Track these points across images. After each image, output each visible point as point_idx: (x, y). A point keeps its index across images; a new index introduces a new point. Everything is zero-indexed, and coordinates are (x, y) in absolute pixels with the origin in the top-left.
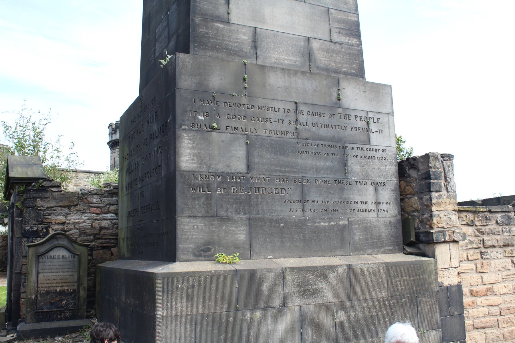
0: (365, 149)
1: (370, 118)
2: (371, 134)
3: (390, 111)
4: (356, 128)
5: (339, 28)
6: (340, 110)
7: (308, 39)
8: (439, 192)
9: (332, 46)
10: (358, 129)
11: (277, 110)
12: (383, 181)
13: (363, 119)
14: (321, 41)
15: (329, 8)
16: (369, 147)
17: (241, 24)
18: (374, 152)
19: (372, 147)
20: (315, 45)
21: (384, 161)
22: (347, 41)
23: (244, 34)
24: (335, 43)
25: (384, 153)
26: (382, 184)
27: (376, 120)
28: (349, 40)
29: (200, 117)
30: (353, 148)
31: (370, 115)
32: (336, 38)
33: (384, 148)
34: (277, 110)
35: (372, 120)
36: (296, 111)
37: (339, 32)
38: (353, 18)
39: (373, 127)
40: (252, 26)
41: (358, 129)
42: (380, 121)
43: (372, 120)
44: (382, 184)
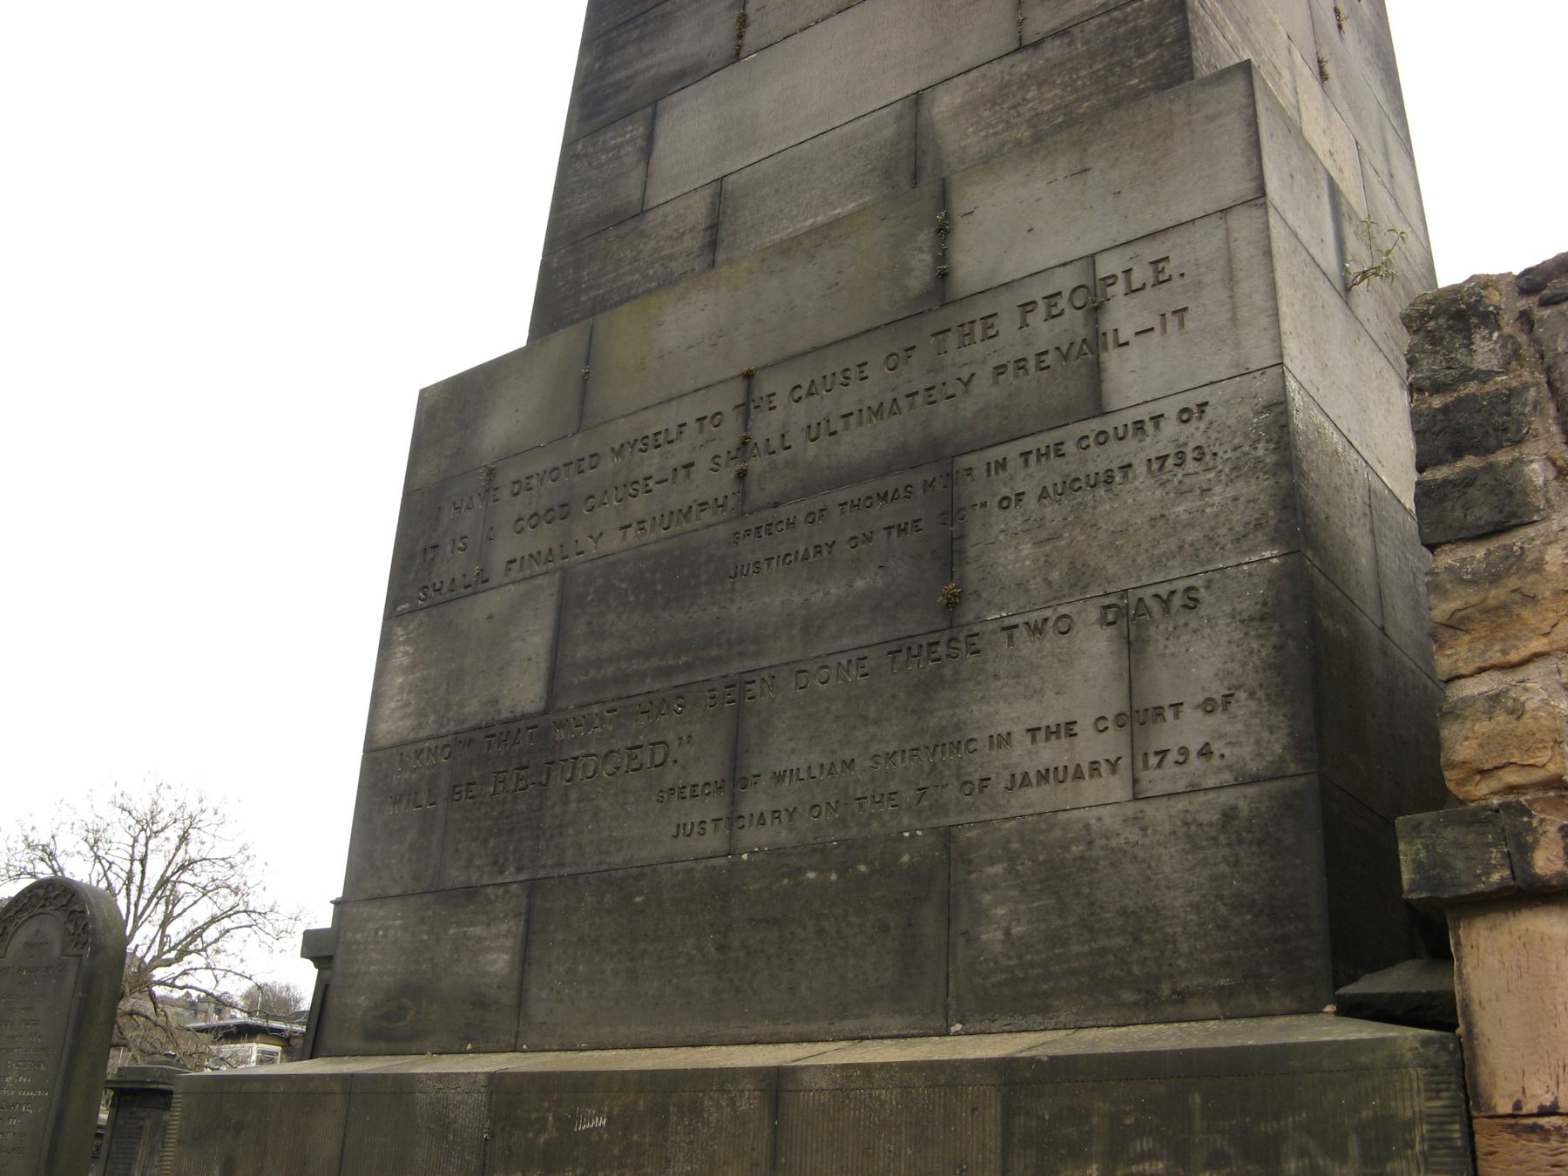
30: (1002, 465)
33: (1191, 400)
35: (1119, 288)
36: (746, 409)
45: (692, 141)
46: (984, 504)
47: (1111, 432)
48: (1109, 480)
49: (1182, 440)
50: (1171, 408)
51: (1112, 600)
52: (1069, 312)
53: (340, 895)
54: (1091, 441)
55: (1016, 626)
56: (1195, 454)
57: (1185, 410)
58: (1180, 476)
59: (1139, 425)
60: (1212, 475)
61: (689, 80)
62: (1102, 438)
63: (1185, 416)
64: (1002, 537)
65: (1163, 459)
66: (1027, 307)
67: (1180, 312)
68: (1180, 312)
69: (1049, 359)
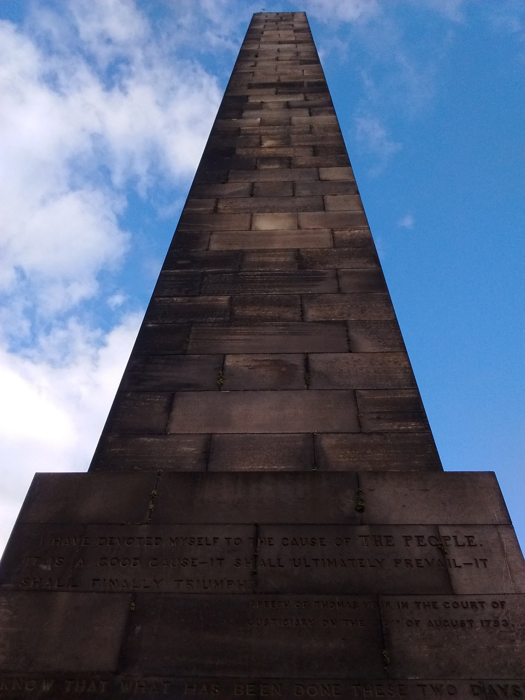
0: (440, 604)
1: (448, 538)
2: (454, 571)
3: (502, 519)
4: (408, 562)
5: (377, 412)
6: (364, 530)
7: (313, 437)
8: (77, 586)
9: (364, 440)
10: (414, 563)
11: (211, 541)
12: (510, 683)
13: (426, 541)
14: (340, 435)
15: (355, 391)
16: (451, 599)
17: (188, 432)
18: (470, 611)
19: (459, 600)
20: (327, 442)
21: (502, 628)
22: (395, 427)
23: (189, 445)
24: (370, 434)
25: (499, 611)
26: (510, 691)
27: (461, 540)
28: (399, 426)
29: (44, 567)
30: (405, 605)
31: (445, 532)
32: (370, 426)
33: (499, 599)
34: (211, 541)
35: (452, 542)
36: (256, 538)
37: (379, 418)
38: (408, 395)
39: (457, 555)
40: (206, 432)
41: (414, 563)
42: (476, 540)
43: (452, 542)
44: (510, 691)
45: (191, 419)
46: (398, 621)
47: (460, 603)
48: (463, 624)
49: (496, 615)
50: (489, 600)
51: (476, 683)
52: (428, 545)
53: (87, 472)
54: (450, 605)
55: (425, 686)
56: (504, 623)
57: (495, 602)
58: (498, 631)
59: (473, 604)
60: (514, 634)
61: (191, 389)
62: (456, 605)
63: (495, 605)
64: (410, 639)
65: (489, 621)
66: (407, 538)
67: (484, 561)
68: (484, 561)
69: (423, 563)
